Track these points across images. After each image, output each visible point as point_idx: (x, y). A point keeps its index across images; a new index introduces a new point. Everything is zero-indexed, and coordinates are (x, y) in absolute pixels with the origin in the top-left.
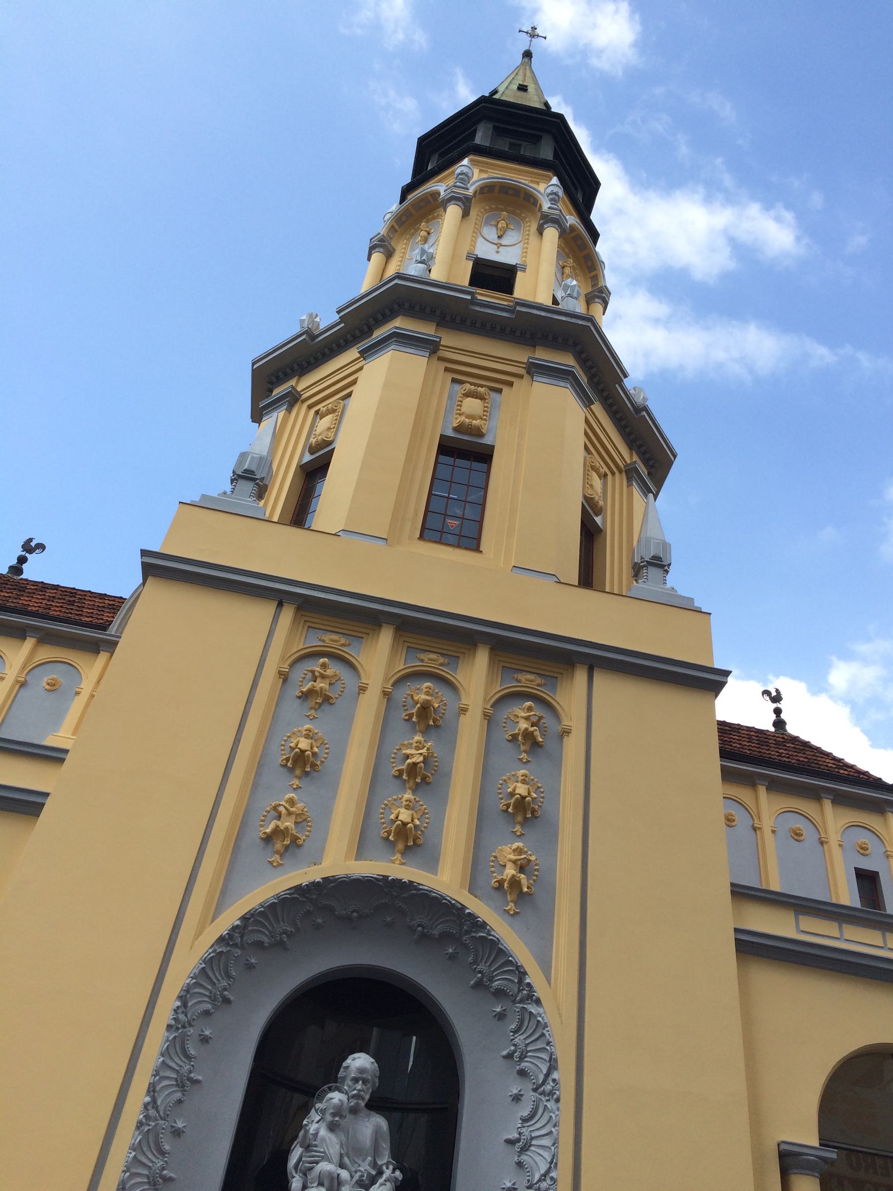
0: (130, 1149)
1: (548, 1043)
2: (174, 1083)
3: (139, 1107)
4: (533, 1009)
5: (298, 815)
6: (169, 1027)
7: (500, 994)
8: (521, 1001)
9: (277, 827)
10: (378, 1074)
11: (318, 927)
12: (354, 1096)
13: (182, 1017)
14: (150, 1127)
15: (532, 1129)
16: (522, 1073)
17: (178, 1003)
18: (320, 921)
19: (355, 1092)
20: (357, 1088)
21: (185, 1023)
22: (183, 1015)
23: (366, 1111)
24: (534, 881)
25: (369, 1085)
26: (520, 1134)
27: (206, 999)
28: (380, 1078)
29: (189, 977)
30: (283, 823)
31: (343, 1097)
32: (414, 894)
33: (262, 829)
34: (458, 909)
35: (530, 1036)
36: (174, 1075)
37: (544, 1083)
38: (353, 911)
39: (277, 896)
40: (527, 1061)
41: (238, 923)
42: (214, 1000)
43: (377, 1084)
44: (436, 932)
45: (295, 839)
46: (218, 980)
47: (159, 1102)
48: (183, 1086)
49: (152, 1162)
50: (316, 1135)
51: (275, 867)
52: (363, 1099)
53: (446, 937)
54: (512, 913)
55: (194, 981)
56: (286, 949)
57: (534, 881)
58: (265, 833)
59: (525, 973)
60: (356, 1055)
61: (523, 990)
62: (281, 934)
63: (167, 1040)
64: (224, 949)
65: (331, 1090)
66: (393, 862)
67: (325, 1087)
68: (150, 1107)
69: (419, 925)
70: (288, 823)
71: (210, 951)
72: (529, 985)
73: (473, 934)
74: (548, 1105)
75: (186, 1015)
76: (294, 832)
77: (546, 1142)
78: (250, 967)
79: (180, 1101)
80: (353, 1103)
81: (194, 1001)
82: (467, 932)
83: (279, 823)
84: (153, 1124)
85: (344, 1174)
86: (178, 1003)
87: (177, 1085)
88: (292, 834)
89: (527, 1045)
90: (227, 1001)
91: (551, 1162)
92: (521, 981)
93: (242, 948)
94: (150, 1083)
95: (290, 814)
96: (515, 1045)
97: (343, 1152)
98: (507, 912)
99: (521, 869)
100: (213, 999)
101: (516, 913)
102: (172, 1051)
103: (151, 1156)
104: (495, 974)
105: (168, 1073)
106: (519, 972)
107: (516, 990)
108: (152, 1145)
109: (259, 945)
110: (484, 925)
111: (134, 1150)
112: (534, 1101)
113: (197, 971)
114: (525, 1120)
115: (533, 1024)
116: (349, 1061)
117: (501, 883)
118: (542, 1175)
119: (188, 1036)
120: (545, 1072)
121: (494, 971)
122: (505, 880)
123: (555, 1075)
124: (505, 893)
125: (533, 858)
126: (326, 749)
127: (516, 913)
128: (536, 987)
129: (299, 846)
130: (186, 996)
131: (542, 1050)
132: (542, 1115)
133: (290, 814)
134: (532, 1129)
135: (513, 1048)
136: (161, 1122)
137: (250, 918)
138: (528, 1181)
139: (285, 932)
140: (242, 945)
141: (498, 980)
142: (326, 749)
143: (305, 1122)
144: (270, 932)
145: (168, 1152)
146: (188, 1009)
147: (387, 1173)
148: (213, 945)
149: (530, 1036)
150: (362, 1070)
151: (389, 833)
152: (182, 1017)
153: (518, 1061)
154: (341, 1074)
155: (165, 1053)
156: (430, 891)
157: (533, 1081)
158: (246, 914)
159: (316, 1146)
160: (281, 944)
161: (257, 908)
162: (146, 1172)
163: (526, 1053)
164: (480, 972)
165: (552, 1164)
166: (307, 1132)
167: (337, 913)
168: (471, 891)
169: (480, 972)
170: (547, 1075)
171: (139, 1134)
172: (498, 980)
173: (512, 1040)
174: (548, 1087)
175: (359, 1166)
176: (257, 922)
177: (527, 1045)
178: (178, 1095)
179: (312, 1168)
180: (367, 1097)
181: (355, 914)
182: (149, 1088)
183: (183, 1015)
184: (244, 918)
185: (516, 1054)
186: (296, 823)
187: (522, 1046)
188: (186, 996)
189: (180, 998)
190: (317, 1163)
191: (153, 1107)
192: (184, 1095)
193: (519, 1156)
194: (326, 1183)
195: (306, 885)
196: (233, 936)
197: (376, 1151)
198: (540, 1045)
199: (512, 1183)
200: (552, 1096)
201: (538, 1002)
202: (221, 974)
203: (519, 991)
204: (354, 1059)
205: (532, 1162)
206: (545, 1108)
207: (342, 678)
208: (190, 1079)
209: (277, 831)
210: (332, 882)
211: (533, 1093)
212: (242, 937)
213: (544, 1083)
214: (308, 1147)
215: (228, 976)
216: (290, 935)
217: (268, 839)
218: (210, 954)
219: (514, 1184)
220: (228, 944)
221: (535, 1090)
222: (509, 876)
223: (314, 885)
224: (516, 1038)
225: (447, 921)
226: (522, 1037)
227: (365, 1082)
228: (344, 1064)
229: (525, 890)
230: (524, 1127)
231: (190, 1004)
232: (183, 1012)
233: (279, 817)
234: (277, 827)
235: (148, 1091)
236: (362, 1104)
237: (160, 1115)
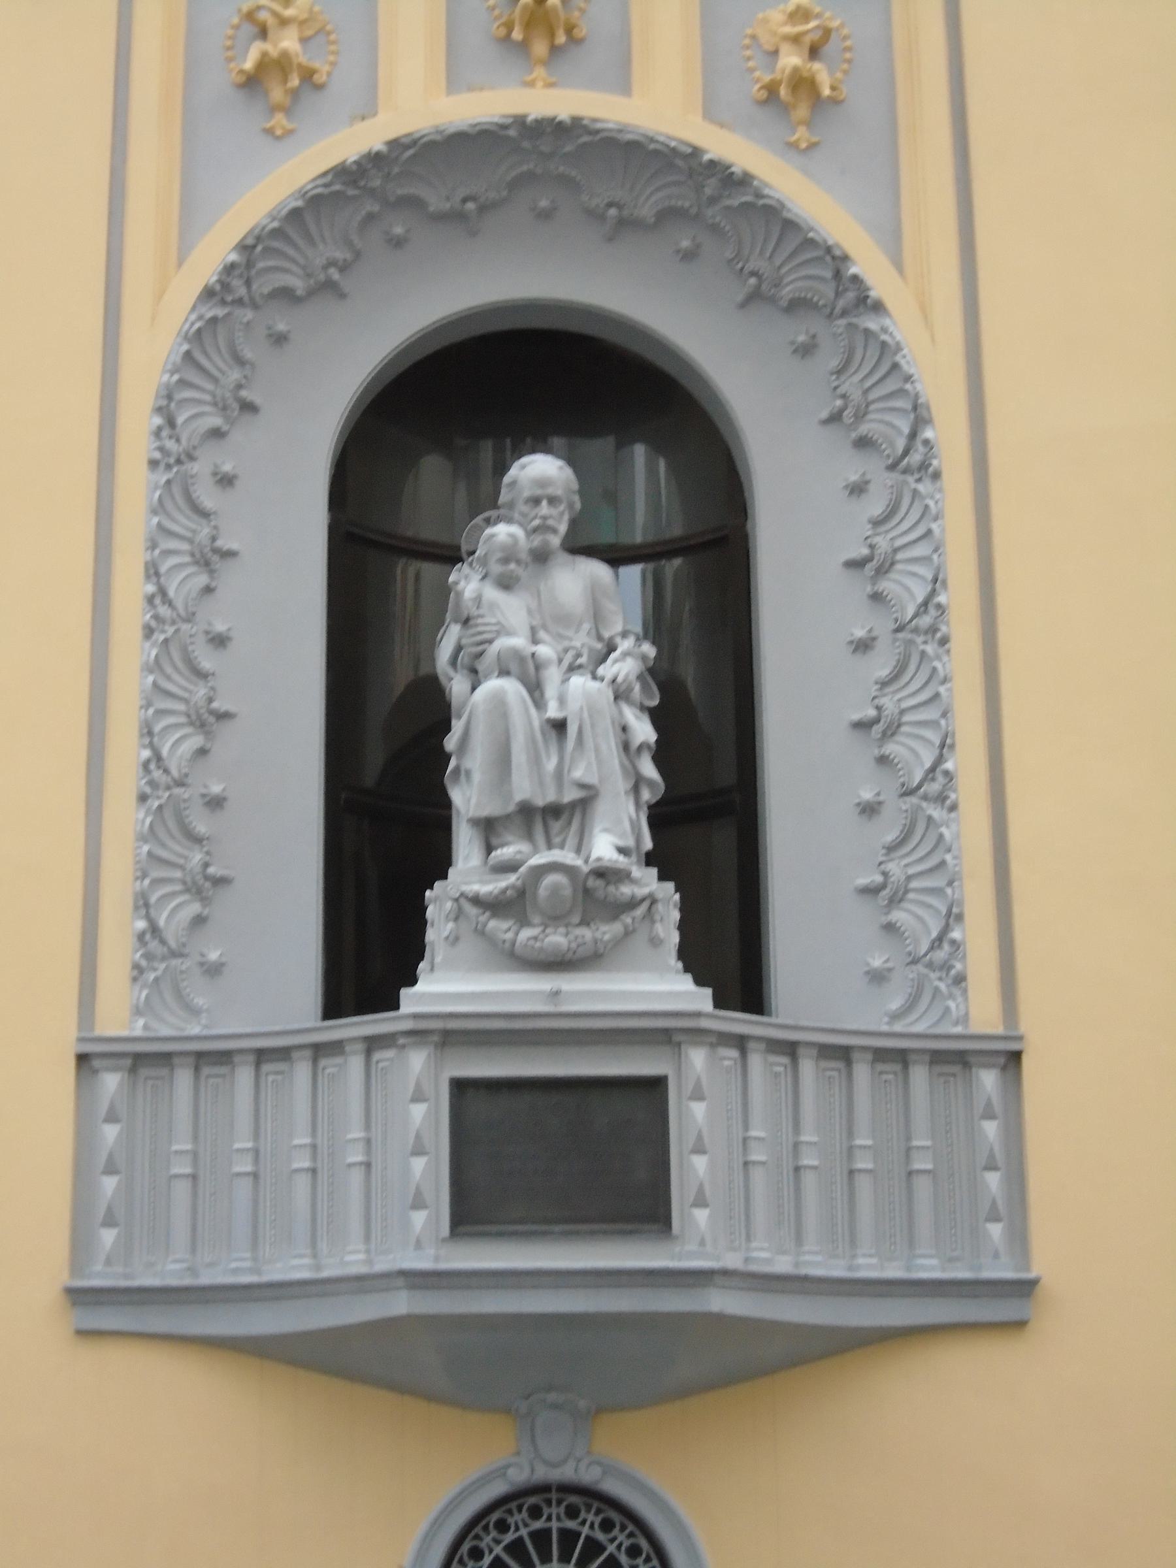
0: (137, 840)
1: (908, 378)
2: (183, 719)
3: (139, 603)
4: (872, 324)
5: (302, 23)
6: (153, 464)
7: (796, 306)
8: (844, 313)
9: (265, 54)
10: (575, 486)
11: (398, 243)
12: (535, 530)
13: (170, 445)
14: (162, 801)
15: (890, 535)
16: (863, 443)
17: (158, 420)
18: (398, 230)
19: (536, 522)
20: (540, 514)
21: (179, 455)
22: (173, 441)
23: (565, 557)
24: (845, 72)
25: (562, 508)
26: (872, 547)
27: (208, 409)
28: (582, 492)
29: (164, 372)
30: (275, 45)
31: (515, 529)
32: (585, 144)
33: (232, 65)
34: (686, 157)
35: (921, 860)
36: (185, 546)
37: (906, 452)
38: (465, 200)
39: (301, 193)
40: (872, 421)
41: (233, 257)
42: (225, 408)
43: (578, 505)
44: (647, 211)
45: (308, 75)
46: (223, 373)
47: (171, 593)
48: (207, 564)
49: (186, 689)
50: (478, 600)
51: (278, 138)
52: (554, 531)
53: (668, 215)
54: (803, 145)
55: (176, 377)
56: (342, 296)
57: (845, 72)
58: (241, 72)
59: (845, 258)
60: (525, 460)
61: (846, 290)
62: (325, 268)
63: (156, 488)
64: (220, 312)
65: (488, 522)
66: (531, 84)
67: (479, 519)
68: (152, 766)
69: (610, 205)
70: (288, 42)
71: (193, 317)
72: (855, 279)
73: (728, 202)
74: (921, 487)
75: (178, 440)
76: (303, 60)
77: (920, 550)
78: (280, 339)
79: (202, 752)
80: (537, 541)
81: (165, 915)
82: (713, 201)
83: (267, 46)
84: (167, 794)
85: (545, 651)
86: (158, 420)
87: (191, 724)
88: (300, 66)
89: (866, 392)
90: (249, 408)
91: (935, 580)
92: (838, 274)
93: (255, 306)
94: (146, 564)
95: (284, 22)
96: (844, 396)
97: (534, 623)
98: (794, 146)
99: (814, 52)
100: (223, 408)
101: (813, 146)
102: (162, 833)
103: (178, 848)
104: (784, 270)
105: (173, 544)
106: (834, 258)
107: (831, 295)
108: (180, 664)
109: (285, 294)
110: (744, 181)
111: (151, 672)
112: (892, 487)
113: (178, 359)
114: (877, 523)
115: (873, 353)
116: (514, 472)
117: (771, 90)
118: (920, 606)
119: (185, 801)
120: (906, 430)
121: (779, 268)
122: (780, 83)
123: (929, 434)
124: (785, 109)
125: (835, 24)
126: (333, 53)
127: (813, 146)
128: (870, 279)
129: (320, 87)
130: (168, 406)
131: (900, 393)
132: (907, 514)
133: (284, 22)
134: (890, 535)
135: (839, 403)
136: (185, 627)
137: (254, 247)
138: (896, 620)
139: (332, 263)
140: (252, 299)
141: (791, 282)
142: (333, 53)
143: (451, 579)
144: (304, 268)
145: (207, 835)
146: (178, 429)
147: (625, 645)
148: (194, 308)
149: (921, 860)
150: (542, 483)
151: (509, 27)
152: (170, 445)
153: (851, 424)
154: (504, 497)
155: (159, 508)
156: (620, 131)
157: (886, 453)
158: (245, 237)
159: (482, 616)
160: (329, 286)
161: (265, 222)
162: (181, 707)
163: (867, 406)
164: (753, 274)
165: (936, 583)
166: (459, 595)
167: (431, 209)
168: (709, 114)
169: (753, 274)
170: (913, 435)
171: (153, 645)
172: (791, 282)
173: (836, 388)
174: (915, 458)
175: (571, 639)
176: (268, 251)
177: (866, 392)
178: (195, 908)
179: (481, 654)
180: (563, 528)
181: (470, 206)
182: (147, 570)
183: (173, 441)
184: (244, 247)
185: (845, 413)
186: (304, 41)
187: (856, 396)
188: (168, 406)
189: (159, 410)
190: (490, 642)
191: (159, 767)
192: (204, 906)
193: (874, 584)
194: (514, 667)
195: (355, 162)
196: (228, 284)
197: (598, 616)
198: (891, 385)
199: (867, 629)
200: (926, 471)
201: (878, 307)
202: (224, 361)
203: (838, 294)
204: (523, 467)
205: (882, 428)
206: (914, 493)
207: (329, 28)
208: (216, 551)
209: (264, 64)
210: (407, 147)
211: (887, 474)
212: (248, 283)
213: (906, 452)
214: (466, 622)
215: (240, 361)
216: (344, 268)
217: (252, 82)
218: (193, 324)
219: (870, 631)
220: (223, 302)
221: (892, 467)
222: (787, 71)
223: (375, 159)
224: (844, 382)
225: (664, 186)
226: (856, 378)
227: (552, 501)
228: (506, 479)
229: (826, 92)
230: (878, 534)
231: (180, 420)
232: (170, 437)
233: (263, 33)
234: (265, 54)
235: (148, 577)
236: (555, 541)
237: (179, 615)
